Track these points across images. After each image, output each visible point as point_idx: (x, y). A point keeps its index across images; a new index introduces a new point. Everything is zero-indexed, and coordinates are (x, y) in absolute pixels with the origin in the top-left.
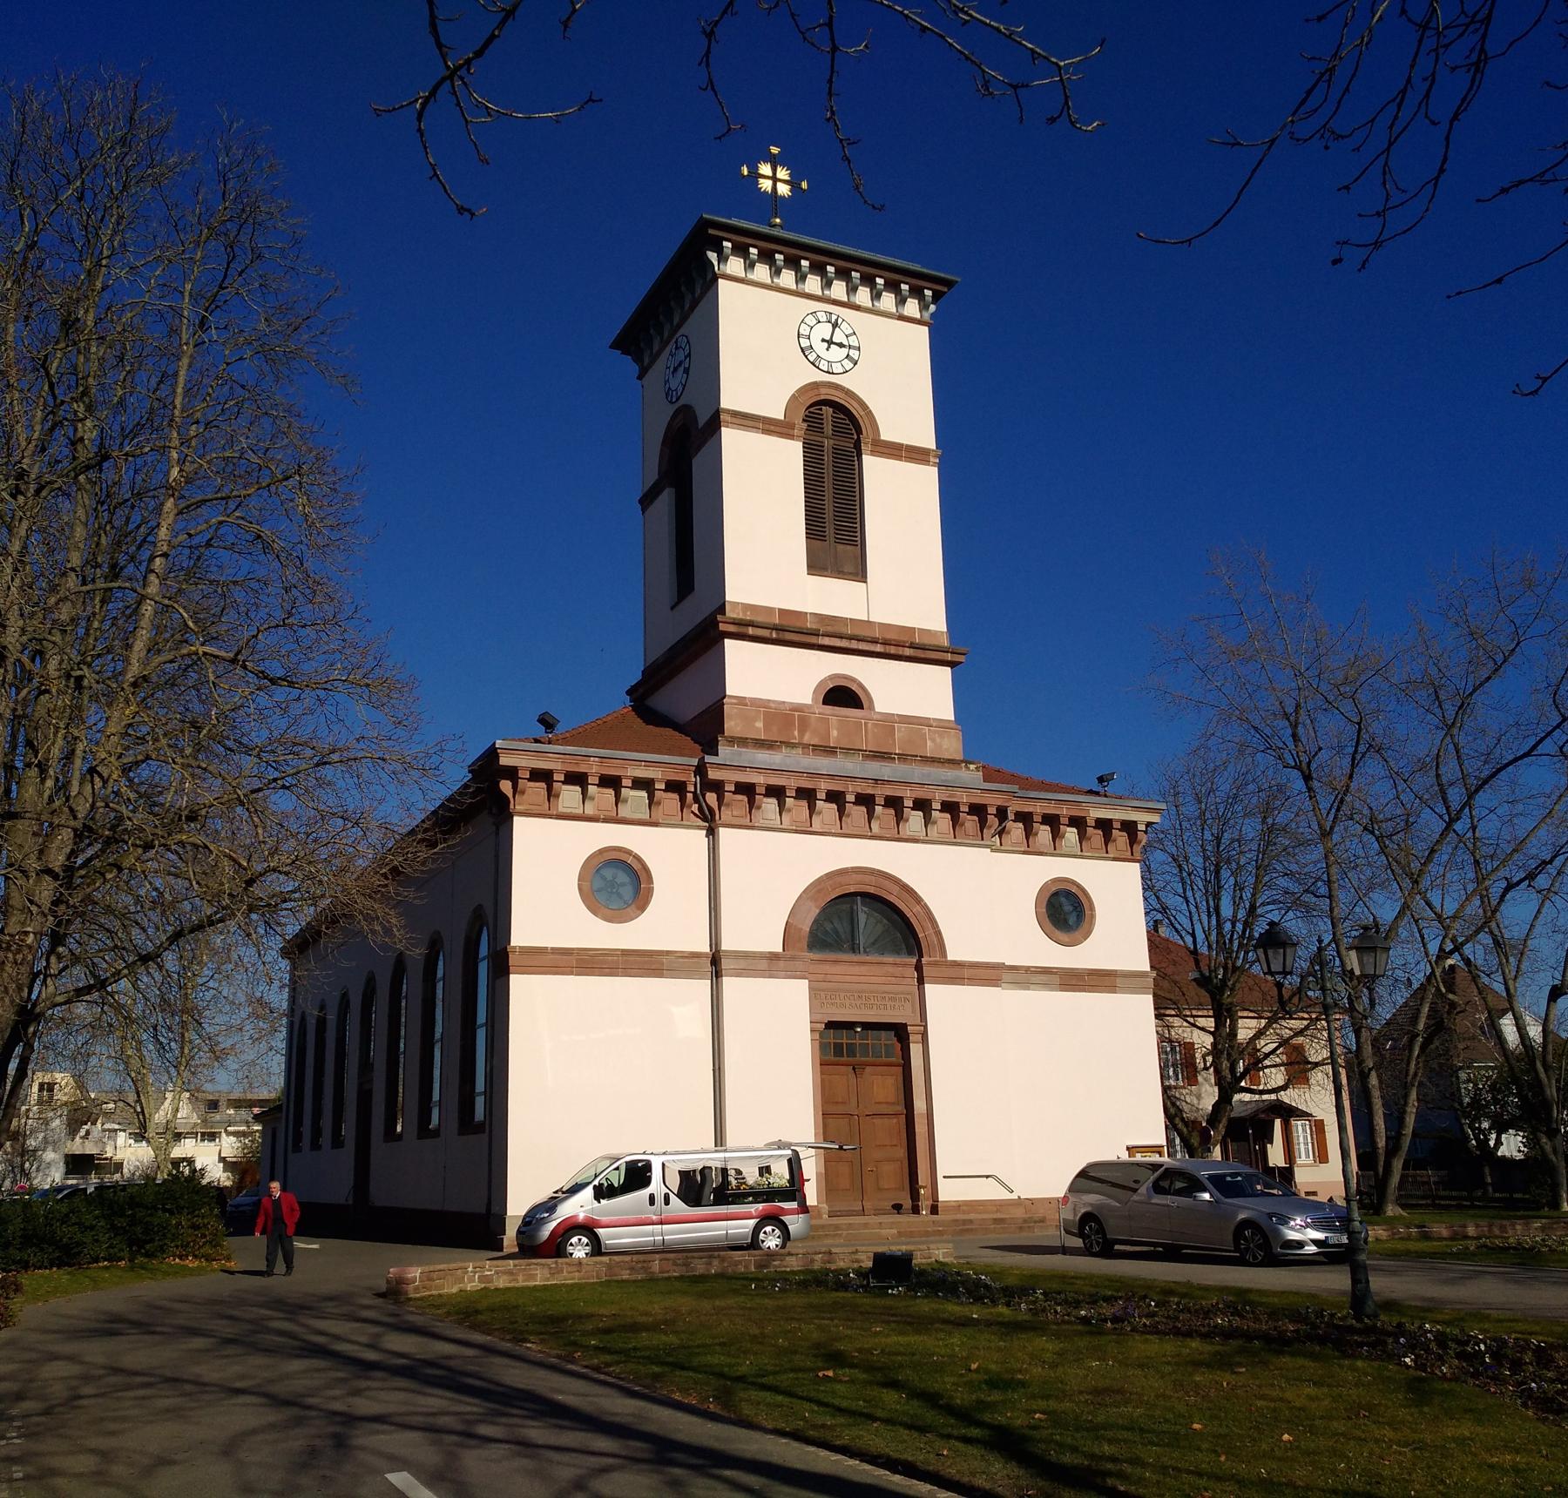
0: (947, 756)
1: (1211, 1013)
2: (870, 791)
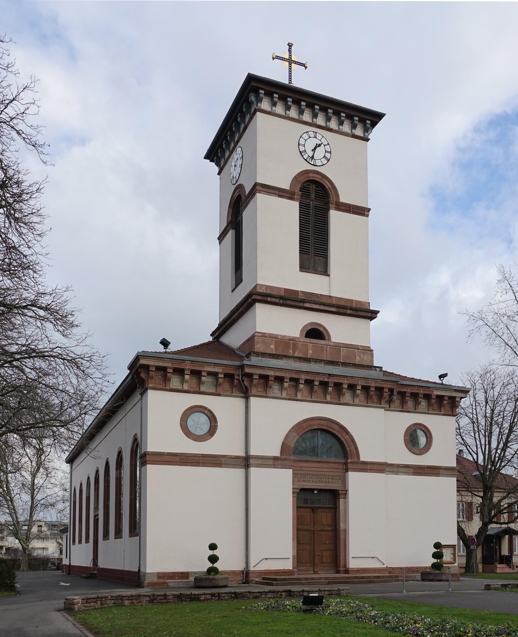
0: (366, 364)
1: (482, 490)
2: (326, 380)
